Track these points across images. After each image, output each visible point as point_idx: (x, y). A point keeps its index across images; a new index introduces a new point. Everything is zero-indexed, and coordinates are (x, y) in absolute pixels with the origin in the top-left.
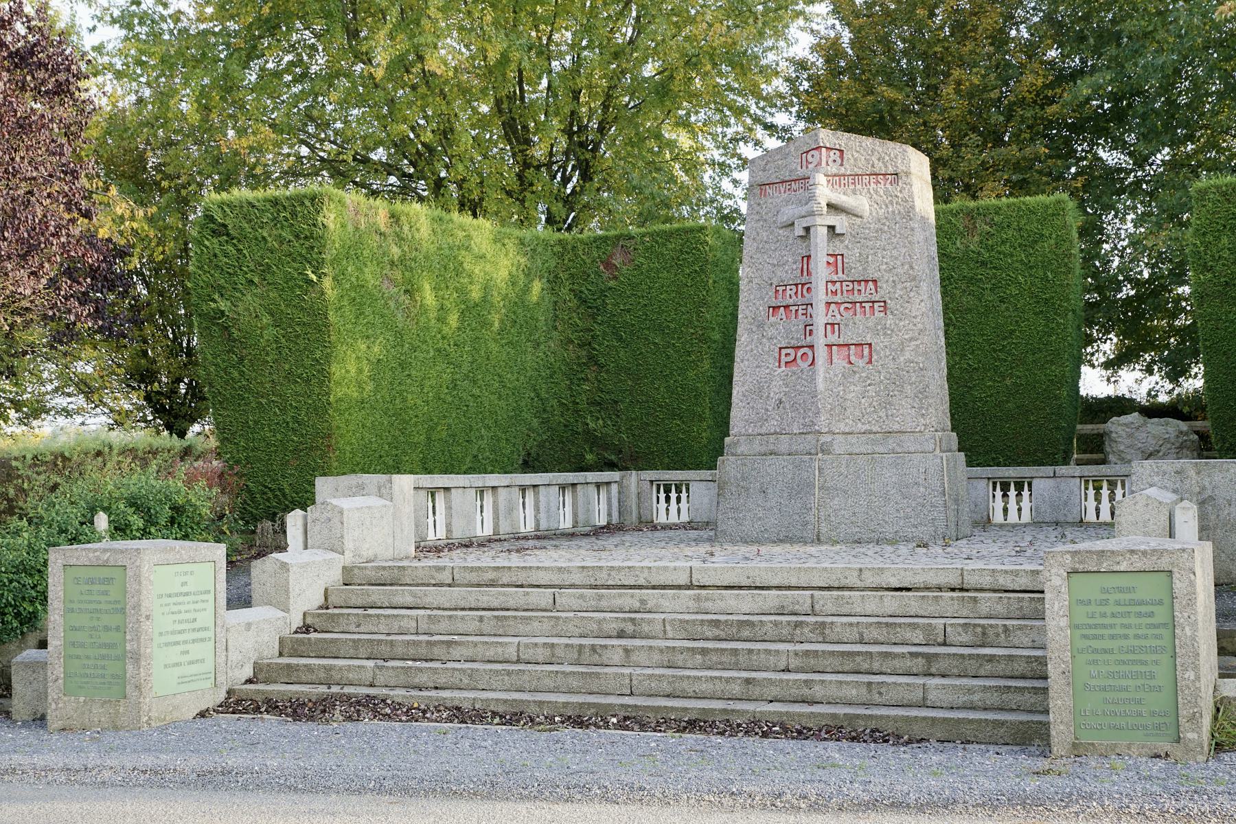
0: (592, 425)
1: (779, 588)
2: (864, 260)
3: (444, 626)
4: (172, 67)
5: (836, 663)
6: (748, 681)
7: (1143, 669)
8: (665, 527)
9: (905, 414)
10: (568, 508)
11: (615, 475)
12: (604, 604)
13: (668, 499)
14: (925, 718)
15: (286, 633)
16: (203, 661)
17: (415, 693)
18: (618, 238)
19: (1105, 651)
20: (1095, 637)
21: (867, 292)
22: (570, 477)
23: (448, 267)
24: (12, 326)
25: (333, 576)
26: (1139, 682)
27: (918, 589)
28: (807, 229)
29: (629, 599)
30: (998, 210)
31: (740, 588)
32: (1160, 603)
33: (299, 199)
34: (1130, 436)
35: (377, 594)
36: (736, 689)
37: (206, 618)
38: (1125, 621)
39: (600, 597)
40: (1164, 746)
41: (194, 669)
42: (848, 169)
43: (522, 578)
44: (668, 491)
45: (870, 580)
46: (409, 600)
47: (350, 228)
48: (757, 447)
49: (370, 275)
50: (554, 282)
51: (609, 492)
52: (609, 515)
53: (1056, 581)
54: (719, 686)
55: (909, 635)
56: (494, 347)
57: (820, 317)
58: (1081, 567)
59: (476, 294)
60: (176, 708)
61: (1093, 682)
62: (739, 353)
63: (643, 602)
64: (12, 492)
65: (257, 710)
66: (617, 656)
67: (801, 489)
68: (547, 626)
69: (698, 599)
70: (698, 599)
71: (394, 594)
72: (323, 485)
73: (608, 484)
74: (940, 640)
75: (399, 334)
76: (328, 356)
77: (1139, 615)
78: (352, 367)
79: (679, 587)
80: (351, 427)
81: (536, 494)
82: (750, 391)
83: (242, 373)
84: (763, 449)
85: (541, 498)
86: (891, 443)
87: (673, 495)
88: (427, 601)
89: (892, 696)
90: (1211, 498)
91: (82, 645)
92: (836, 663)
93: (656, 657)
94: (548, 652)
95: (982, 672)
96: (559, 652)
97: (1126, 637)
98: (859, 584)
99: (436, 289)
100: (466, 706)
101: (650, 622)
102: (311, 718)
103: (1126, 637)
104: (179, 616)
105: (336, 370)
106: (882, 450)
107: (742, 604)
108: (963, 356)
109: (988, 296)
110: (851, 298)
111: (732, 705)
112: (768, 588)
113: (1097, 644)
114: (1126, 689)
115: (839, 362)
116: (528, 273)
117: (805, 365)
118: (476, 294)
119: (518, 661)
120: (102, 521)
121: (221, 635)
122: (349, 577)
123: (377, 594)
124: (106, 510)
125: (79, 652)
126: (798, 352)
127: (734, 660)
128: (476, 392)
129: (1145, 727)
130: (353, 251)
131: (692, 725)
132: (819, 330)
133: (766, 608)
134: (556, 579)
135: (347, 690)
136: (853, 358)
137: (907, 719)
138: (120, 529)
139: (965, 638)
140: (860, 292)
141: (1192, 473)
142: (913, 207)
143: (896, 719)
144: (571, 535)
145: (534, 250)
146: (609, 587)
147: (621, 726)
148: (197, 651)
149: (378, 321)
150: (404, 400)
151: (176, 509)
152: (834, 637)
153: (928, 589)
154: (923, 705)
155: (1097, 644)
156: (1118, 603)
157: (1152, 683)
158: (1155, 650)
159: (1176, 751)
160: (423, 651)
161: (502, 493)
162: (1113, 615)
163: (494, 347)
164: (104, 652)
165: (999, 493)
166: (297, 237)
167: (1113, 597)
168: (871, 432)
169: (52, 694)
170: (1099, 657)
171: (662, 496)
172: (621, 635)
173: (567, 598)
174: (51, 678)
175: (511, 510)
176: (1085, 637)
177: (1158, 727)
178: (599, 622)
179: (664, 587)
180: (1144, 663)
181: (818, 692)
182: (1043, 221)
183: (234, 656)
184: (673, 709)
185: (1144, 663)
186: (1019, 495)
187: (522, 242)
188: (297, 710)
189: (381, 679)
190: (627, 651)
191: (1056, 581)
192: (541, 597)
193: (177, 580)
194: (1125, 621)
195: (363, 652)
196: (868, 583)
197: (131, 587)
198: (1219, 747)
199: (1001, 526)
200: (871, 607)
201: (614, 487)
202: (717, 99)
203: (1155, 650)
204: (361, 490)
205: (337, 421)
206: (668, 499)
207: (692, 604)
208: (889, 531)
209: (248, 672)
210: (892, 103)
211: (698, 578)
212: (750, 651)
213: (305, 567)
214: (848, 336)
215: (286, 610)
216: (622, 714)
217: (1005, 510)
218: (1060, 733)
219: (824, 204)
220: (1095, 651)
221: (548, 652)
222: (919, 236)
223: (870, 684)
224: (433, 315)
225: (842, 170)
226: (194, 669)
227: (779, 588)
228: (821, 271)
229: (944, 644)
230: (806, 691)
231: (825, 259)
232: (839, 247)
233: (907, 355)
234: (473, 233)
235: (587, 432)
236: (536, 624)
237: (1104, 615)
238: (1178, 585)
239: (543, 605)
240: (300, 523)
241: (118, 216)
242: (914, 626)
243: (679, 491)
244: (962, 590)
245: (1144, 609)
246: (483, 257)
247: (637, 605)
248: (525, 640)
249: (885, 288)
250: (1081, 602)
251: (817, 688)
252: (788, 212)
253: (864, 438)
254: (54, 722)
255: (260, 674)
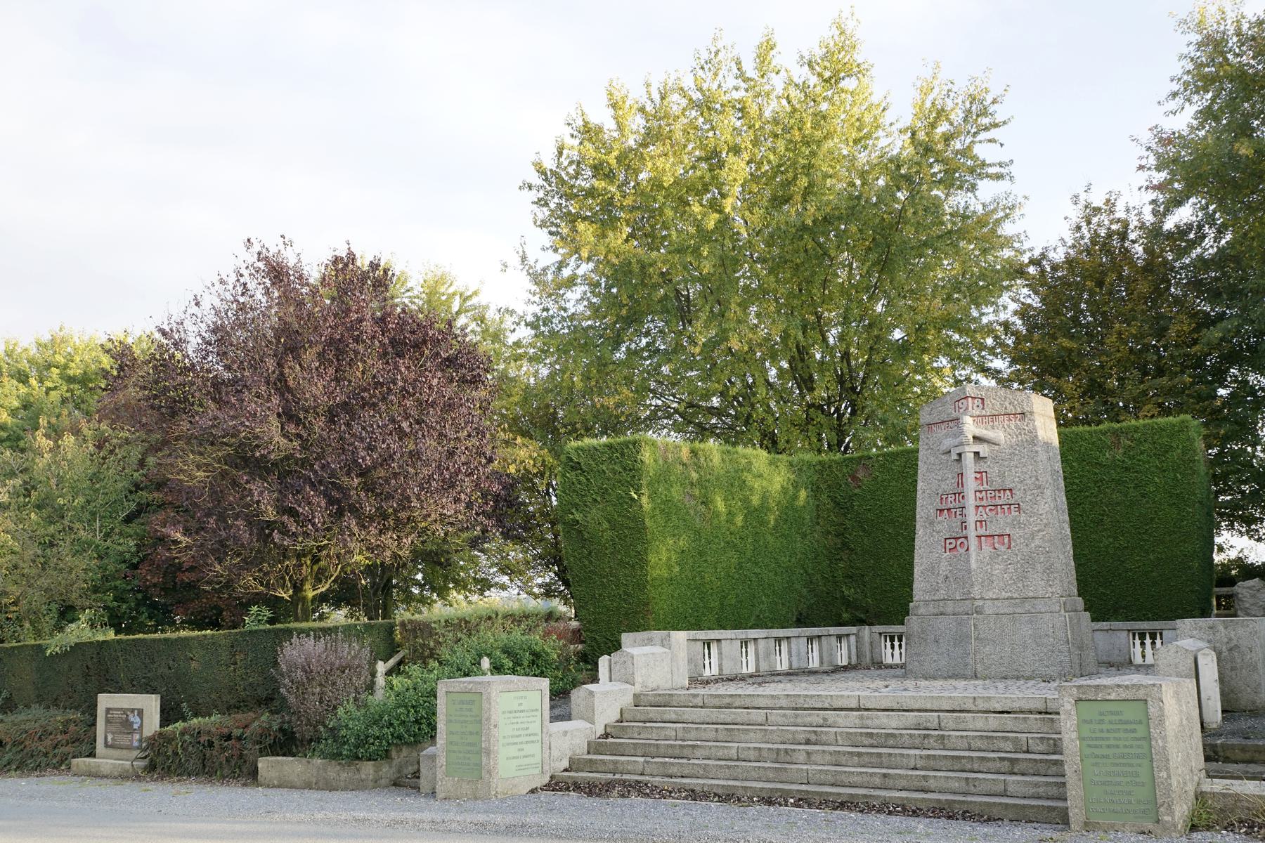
0: (846, 592)
1: (919, 711)
2: (1002, 475)
3: (693, 735)
4: (566, 352)
5: (948, 764)
6: (885, 775)
7: (1130, 769)
8: (891, 667)
9: (1036, 585)
10: (816, 653)
11: (853, 629)
12: (799, 721)
13: (893, 647)
14: (1000, 804)
15: (593, 738)
16: (533, 756)
17: (666, 779)
18: (860, 458)
19: (1104, 757)
20: (1096, 747)
21: (1005, 498)
22: (815, 631)
23: (735, 483)
24: (446, 534)
25: (628, 700)
26: (1129, 779)
27: (1015, 712)
28: (960, 455)
29: (816, 717)
30: (1136, 429)
31: (893, 710)
32: (1140, 722)
33: (626, 444)
34: (1253, 596)
35: (653, 712)
36: (877, 781)
37: (535, 727)
38: (1117, 735)
39: (797, 716)
40: (1149, 826)
41: (527, 761)
42: (988, 411)
43: (748, 702)
44: (892, 640)
45: (982, 705)
46: (673, 717)
47: (661, 462)
48: (931, 610)
49: (676, 493)
50: (815, 490)
51: (848, 641)
52: (850, 658)
53: (1068, 707)
54: (866, 779)
55: (1002, 745)
56: (771, 539)
57: (972, 517)
58: (1084, 697)
59: (756, 500)
60: (514, 786)
61: (1097, 779)
62: (917, 543)
63: (825, 720)
64: (432, 644)
65: (568, 789)
66: (802, 757)
67: (962, 639)
68: (759, 735)
69: (861, 718)
70: (861, 718)
71: (664, 712)
72: (626, 638)
73: (848, 635)
74: (1025, 748)
75: (698, 533)
76: (646, 549)
77: (1126, 731)
78: (663, 557)
79: (852, 710)
80: (664, 597)
81: (789, 644)
82: (926, 569)
83: (591, 562)
84: (936, 611)
85: (793, 646)
86: (1027, 606)
87: (896, 643)
88: (685, 717)
89: (982, 788)
90: (1237, 646)
91: (457, 744)
92: (948, 764)
93: (828, 758)
94: (757, 754)
95: (1050, 772)
96: (765, 754)
97: (1118, 747)
98: (974, 708)
99: (725, 500)
100: (698, 789)
101: (826, 733)
102: (599, 795)
103: (1118, 747)
104: (517, 728)
105: (652, 558)
106: (1020, 611)
107: (892, 722)
108: (1116, 538)
109: (1132, 493)
110: (994, 502)
111: (873, 792)
112: (912, 711)
113: (1097, 751)
114: (1119, 784)
115: (987, 548)
116: (796, 486)
117: (962, 551)
118: (756, 500)
119: (738, 760)
120: (486, 663)
121: (546, 738)
122: (638, 700)
123: (653, 712)
124: (489, 655)
125: (455, 748)
126: (958, 541)
127: (879, 761)
128: (757, 570)
129: (1135, 812)
130: (664, 475)
131: (842, 805)
132: (971, 526)
133: (908, 724)
134: (770, 703)
135: (625, 777)
136: (997, 545)
137: (988, 804)
138: (497, 669)
139: (1042, 748)
140: (1000, 497)
141: (1221, 628)
142: (1036, 436)
143: (980, 804)
144: (788, 674)
145: (800, 470)
146: (805, 709)
147: (795, 805)
148: (529, 749)
149: (681, 523)
150: (703, 578)
151: (534, 654)
152: (949, 745)
153: (1022, 712)
154: (1004, 794)
155: (1097, 751)
156: (1111, 722)
157: (1138, 780)
158: (1138, 756)
159: (1157, 829)
160: (677, 752)
161: (762, 643)
162: (1108, 731)
163: (771, 539)
164: (469, 748)
165: (1138, 642)
166: (625, 469)
167: (1107, 718)
168: (1012, 598)
169: (439, 776)
170: (1098, 760)
171: (889, 644)
172: (808, 742)
173: (775, 716)
174: (439, 764)
175: (768, 655)
176: (1089, 746)
177: (1144, 812)
178: (794, 733)
179: (842, 709)
180: (1131, 765)
181: (932, 784)
182: (1171, 436)
183: (555, 753)
184: (831, 793)
185: (1131, 765)
186: (1153, 643)
187: (791, 465)
188: (591, 790)
189: (648, 770)
190: (808, 753)
191: (1068, 707)
192: (758, 716)
193: (516, 703)
194: (1117, 735)
195: (639, 752)
196: (980, 708)
197: (485, 706)
198: (1194, 828)
199: (1140, 666)
200: (980, 724)
201: (853, 638)
202: (948, 348)
203: (1138, 756)
204: (650, 642)
205: (653, 594)
206: (893, 647)
207: (857, 721)
208: (1027, 671)
209: (566, 764)
210: (1070, 351)
211: (864, 704)
212: (890, 755)
213: (606, 697)
214: (993, 529)
215: (593, 723)
216: (798, 796)
217: (1144, 656)
218: (1076, 815)
219: (970, 437)
220: (1097, 756)
221: (757, 754)
222: (1042, 456)
223: (967, 779)
224: (723, 518)
225: (984, 413)
226: (527, 761)
227: (919, 711)
228: (971, 484)
229: (1028, 752)
230: (924, 783)
231: (974, 475)
232: (983, 467)
233: (1037, 542)
234: (754, 461)
235: (843, 597)
236: (752, 734)
237: (1102, 731)
238: (1151, 710)
239: (759, 721)
240: (607, 664)
241: (524, 454)
242: (1006, 739)
243: (900, 640)
244: (1046, 713)
245: (1129, 727)
246: (761, 476)
247: (821, 722)
248: (743, 745)
249: (1018, 494)
250: (1085, 721)
251: (931, 781)
252: (947, 443)
253: (1006, 602)
254: (440, 795)
255: (574, 765)
